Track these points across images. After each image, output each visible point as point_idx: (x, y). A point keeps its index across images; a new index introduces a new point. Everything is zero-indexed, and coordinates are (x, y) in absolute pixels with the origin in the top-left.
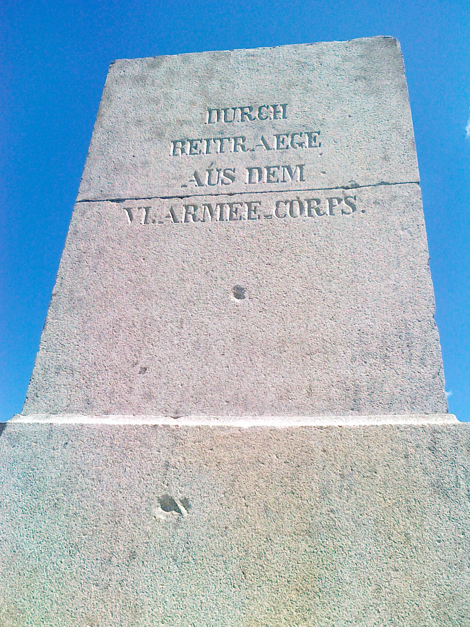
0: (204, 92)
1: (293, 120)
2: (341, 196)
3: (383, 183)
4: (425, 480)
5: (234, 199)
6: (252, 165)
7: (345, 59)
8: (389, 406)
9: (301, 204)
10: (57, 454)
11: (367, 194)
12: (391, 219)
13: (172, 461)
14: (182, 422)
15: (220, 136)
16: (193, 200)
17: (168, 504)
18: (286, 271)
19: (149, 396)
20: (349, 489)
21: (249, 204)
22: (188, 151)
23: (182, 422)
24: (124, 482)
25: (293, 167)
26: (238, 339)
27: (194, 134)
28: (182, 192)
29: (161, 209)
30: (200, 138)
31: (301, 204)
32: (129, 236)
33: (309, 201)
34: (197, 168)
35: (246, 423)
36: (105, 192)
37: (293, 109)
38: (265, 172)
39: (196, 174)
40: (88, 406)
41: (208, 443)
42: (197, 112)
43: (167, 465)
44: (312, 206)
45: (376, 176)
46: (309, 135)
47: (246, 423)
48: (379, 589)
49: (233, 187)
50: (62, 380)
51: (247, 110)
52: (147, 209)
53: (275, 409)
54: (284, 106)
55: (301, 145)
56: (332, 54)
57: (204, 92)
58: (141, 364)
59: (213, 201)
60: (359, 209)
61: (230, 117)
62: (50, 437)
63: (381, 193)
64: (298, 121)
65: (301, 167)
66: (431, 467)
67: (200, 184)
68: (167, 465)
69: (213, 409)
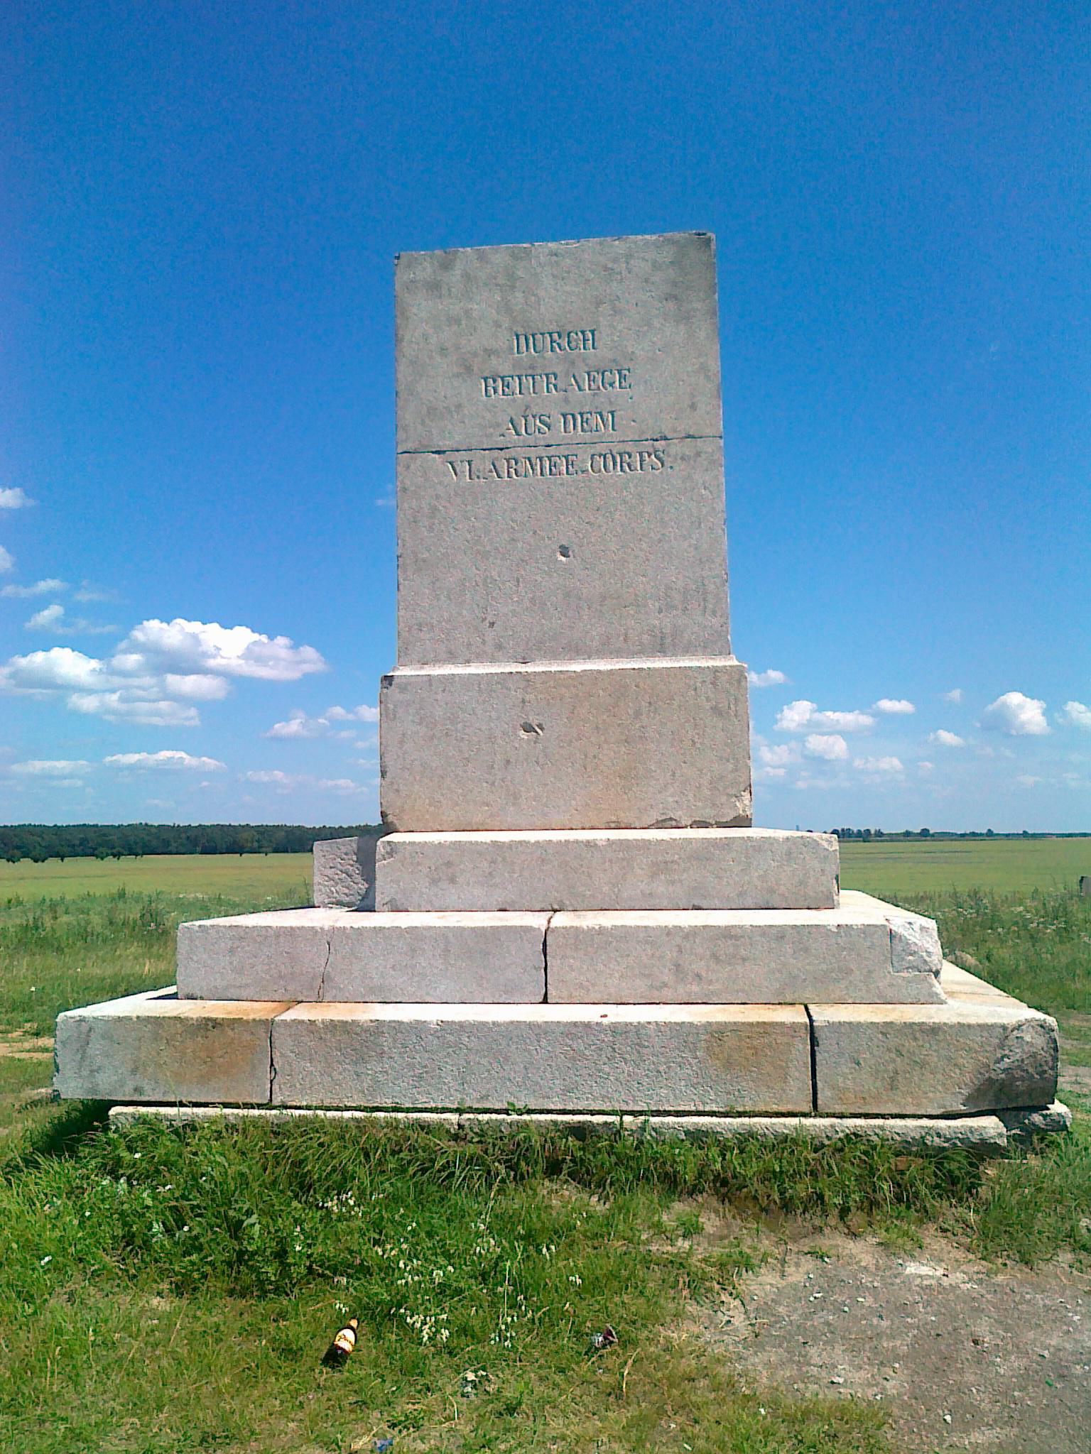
0: (507, 308)
1: (602, 353)
2: (651, 450)
3: (689, 436)
4: (708, 706)
5: (552, 451)
6: (567, 410)
7: (656, 266)
8: (688, 650)
9: (613, 457)
10: (439, 697)
11: (676, 448)
12: (696, 477)
13: (527, 698)
14: (530, 668)
15: (530, 372)
16: (512, 453)
17: (528, 728)
18: (603, 529)
19: (499, 647)
20: (655, 713)
21: (566, 457)
22: (500, 391)
23: (530, 668)
24: (493, 714)
25: (605, 414)
26: (567, 595)
27: (505, 369)
28: (500, 441)
29: (483, 462)
30: (511, 373)
31: (613, 457)
32: (456, 494)
33: (621, 455)
34: (512, 413)
35: (577, 667)
36: (425, 443)
37: (604, 338)
38: (579, 417)
39: (512, 421)
40: (452, 658)
41: (552, 683)
42: (503, 340)
43: (523, 701)
44: (621, 459)
45: (684, 426)
46: (619, 372)
47: (577, 667)
48: (674, 774)
49: (549, 437)
50: (425, 635)
51: (556, 336)
52: (470, 463)
53: (600, 653)
54: (593, 332)
55: (611, 385)
56: (643, 252)
57: (507, 308)
58: (490, 619)
59: (533, 453)
60: (667, 464)
61: (540, 345)
62: (431, 685)
63: (687, 448)
64: (610, 355)
65: (612, 413)
66: (712, 696)
67: (518, 434)
68: (523, 701)
69: (554, 656)
